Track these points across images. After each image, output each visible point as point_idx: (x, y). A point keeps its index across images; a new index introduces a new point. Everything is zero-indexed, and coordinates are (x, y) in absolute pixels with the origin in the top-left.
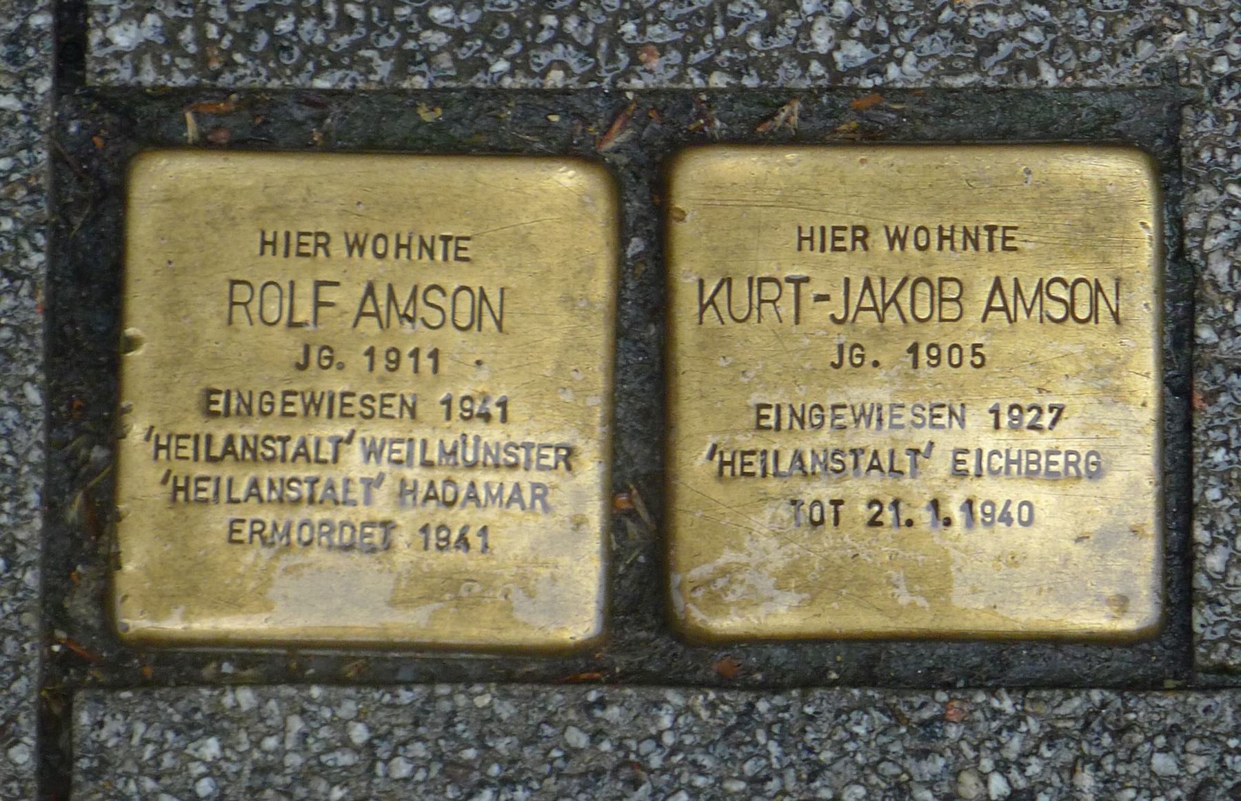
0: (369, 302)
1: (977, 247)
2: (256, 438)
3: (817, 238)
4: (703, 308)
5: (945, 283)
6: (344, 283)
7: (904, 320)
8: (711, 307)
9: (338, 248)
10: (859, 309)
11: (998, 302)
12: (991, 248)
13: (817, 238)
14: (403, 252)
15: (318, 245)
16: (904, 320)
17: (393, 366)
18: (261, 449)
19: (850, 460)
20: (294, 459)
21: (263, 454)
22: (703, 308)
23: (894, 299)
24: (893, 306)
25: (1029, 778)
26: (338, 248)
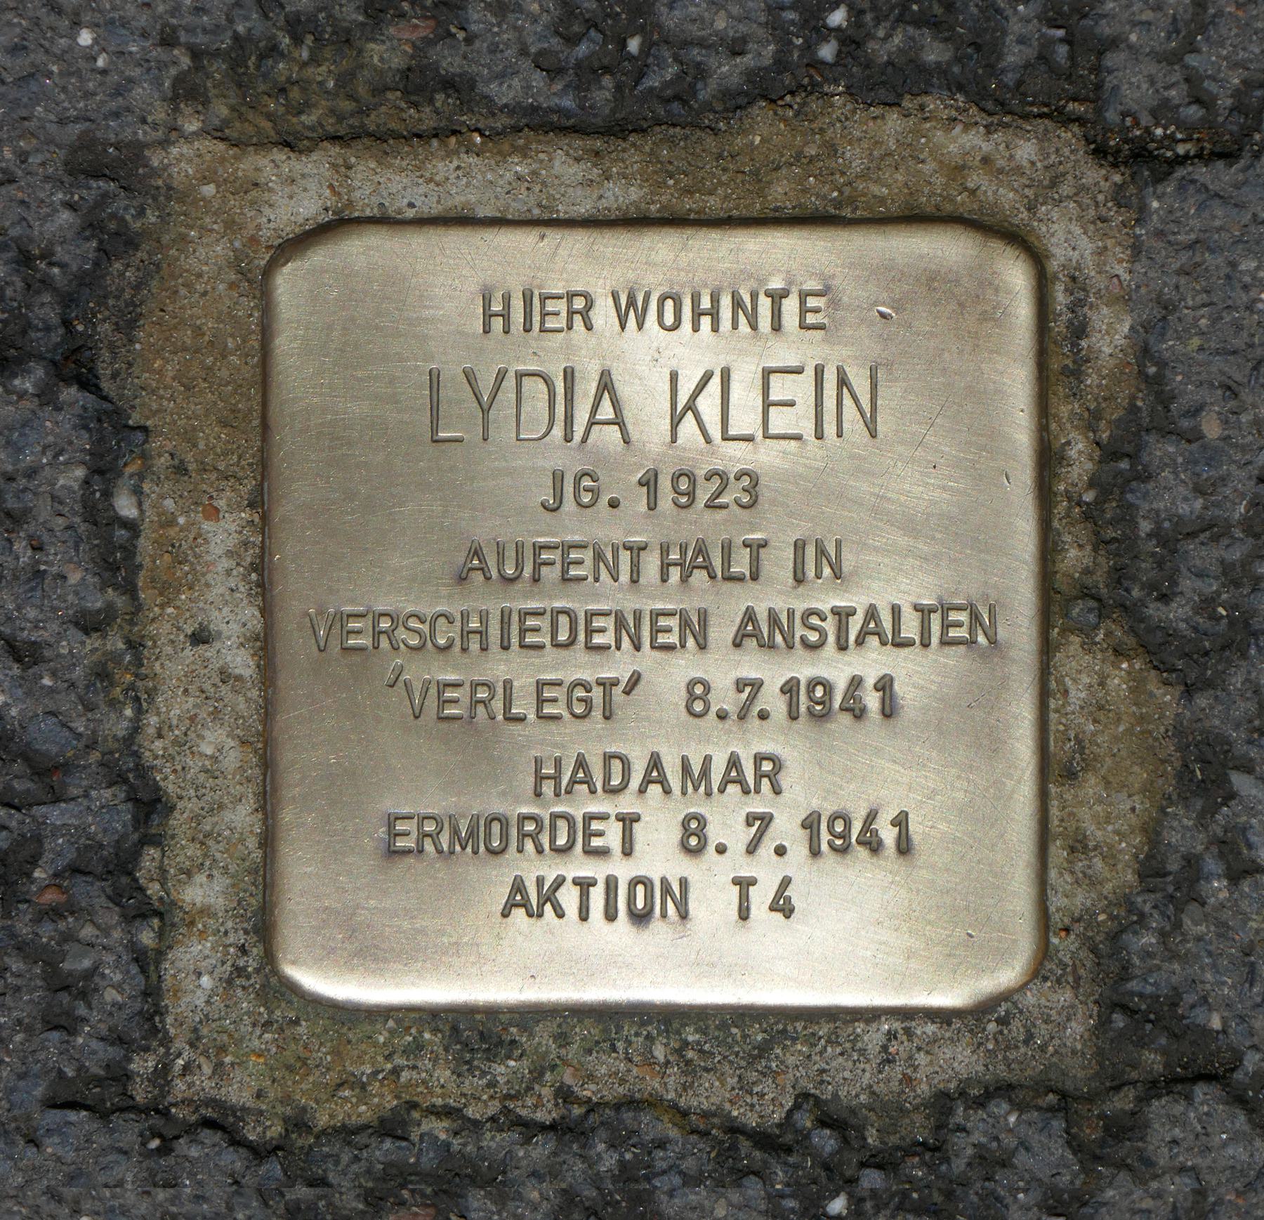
0: (606, 403)
1: (754, 327)
2: (791, 613)
3: (518, 316)
4: (676, 422)
5: (773, 377)
6: (674, 364)
7: (708, 440)
8: (690, 414)
9: (604, 314)
10: (592, 423)
11: (606, 411)
12: (777, 327)
13: (518, 316)
14: (706, 322)
15: (571, 313)
16: (708, 440)
17: (684, 500)
18: (799, 631)
19: (830, 626)
20: (860, 642)
21: (803, 639)
22: (676, 422)
23: (691, 406)
24: (689, 420)
25: (480, 1148)
26: (604, 314)
